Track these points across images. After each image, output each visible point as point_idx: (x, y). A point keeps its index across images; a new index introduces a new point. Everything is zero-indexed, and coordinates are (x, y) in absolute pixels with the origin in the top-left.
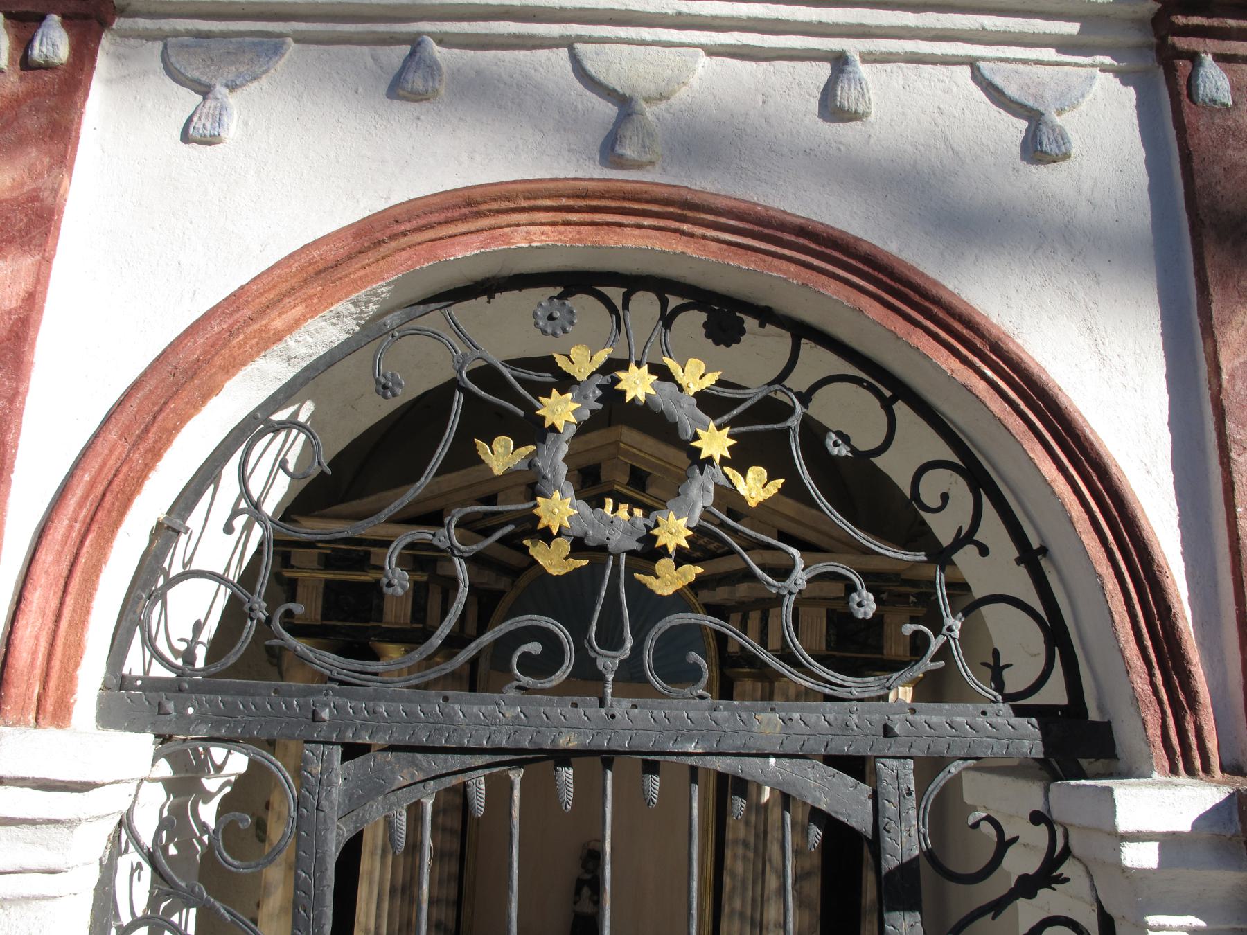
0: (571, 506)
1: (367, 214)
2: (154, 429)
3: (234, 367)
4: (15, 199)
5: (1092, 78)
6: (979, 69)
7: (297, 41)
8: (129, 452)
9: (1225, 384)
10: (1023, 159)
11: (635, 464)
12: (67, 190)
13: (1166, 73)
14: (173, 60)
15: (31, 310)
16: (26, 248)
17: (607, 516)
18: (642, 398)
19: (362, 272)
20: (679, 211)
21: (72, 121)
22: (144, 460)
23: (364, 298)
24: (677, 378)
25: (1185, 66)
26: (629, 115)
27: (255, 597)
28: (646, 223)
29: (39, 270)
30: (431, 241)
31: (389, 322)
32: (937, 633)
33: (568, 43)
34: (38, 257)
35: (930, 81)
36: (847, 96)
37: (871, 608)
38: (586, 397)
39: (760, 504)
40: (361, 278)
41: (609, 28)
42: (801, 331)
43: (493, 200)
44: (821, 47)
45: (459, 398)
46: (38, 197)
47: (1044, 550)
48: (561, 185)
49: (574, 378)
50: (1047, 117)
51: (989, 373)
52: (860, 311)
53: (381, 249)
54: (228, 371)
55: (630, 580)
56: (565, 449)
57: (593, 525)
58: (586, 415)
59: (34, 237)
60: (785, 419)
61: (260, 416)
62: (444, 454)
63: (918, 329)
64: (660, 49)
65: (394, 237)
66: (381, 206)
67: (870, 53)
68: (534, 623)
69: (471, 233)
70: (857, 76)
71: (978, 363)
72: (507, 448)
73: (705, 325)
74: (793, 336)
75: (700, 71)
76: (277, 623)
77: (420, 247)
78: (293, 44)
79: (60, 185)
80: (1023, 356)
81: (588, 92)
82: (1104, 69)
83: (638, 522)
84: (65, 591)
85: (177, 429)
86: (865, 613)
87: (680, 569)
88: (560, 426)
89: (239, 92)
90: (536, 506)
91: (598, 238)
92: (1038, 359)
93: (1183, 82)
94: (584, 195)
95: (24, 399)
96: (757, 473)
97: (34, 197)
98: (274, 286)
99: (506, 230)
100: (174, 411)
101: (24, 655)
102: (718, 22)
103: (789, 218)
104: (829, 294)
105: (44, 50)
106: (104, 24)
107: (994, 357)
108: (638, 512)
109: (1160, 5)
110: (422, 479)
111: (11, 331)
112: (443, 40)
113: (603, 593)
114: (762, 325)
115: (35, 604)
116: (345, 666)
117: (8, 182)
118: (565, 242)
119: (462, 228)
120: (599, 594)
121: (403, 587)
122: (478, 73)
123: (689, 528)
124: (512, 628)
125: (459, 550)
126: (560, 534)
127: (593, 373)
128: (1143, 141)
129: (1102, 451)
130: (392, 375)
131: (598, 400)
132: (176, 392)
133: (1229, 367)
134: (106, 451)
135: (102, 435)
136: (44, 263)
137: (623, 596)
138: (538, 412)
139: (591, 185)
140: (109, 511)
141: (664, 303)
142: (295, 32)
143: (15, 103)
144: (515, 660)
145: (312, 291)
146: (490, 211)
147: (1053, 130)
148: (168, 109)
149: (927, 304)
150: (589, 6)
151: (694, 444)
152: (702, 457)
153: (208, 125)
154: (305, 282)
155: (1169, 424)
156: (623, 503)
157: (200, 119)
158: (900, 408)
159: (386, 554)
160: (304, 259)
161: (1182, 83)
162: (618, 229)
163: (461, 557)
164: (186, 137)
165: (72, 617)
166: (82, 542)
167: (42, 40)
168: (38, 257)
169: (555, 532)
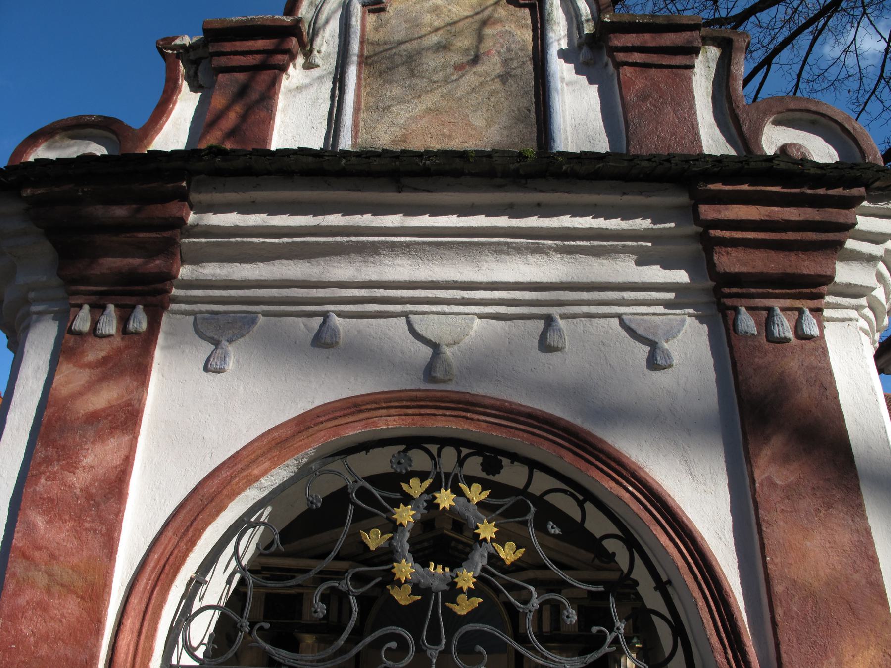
0: (412, 567)
1: (302, 411)
2: (192, 530)
3: (233, 495)
4: (119, 405)
5: (683, 321)
6: (623, 319)
7: (263, 315)
8: (178, 542)
9: (758, 489)
10: (648, 368)
11: (456, 518)
12: (145, 399)
13: (722, 316)
14: (199, 326)
15: (127, 466)
16: (125, 432)
17: (431, 572)
18: (448, 507)
19: (300, 443)
20: (465, 407)
21: (148, 362)
22: (186, 546)
23: (301, 457)
24: (467, 495)
25: (731, 314)
26: (438, 354)
27: (243, 619)
28: (448, 413)
29: (131, 444)
30: (336, 426)
31: (314, 467)
32: (611, 631)
33: (406, 314)
34: (131, 437)
35: (597, 327)
36: (553, 339)
37: (574, 619)
38: (418, 507)
39: (512, 563)
40: (299, 447)
41: (427, 306)
42: (533, 465)
43: (368, 404)
44: (539, 313)
45: (351, 508)
46: (131, 403)
47: (669, 582)
48: (403, 395)
49: (412, 496)
50: (659, 345)
51: (630, 488)
52: (561, 457)
53: (310, 431)
54: (230, 498)
55: (444, 607)
56: (408, 535)
57: (423, 577)
58: (419, 516)
59: (129, 426)
60: (525, 515)
61: (245, 519)
62: (344, 539)
63: (592, 466)
64: (454, 316)
65: (316, 424)
66: (310, 407)
67: (565, 314)
68: (393, 631)
69: (357, 421)
70: (558, 328)
71: (625, 483)
72: (377, 535)
73: (482, 464)
74: (529, 468)
75: (475, 327)
76: (255, 633)
77: (330, 429)
78: (262, 317)
79: (142, 397)
80: (648, 479)
81: (417, 341)
82: (690, 315)
83: (447, 575)
84: (143, 619)
85: (204, 529)
86: (571, 621)
87: (470, 600)
88: (405, 523)
89: (233, 344)
90: (393, 567)
91: (423, 422)
92: (657, 479)
93: (730, 322)
94: (416, 399)
95: (123, 514)
96: (510, 545)
97: (129, 404)
98: (254, 452)
99: (375, 419)
100: (202, 519)
101: (122, 655)
102: (484, 302)
103: (522, 409)
104: (544, 449)
105: (135, 325)
106: (164, 308)
107: (633, 480)
108: (447, 569)
109: (715, 283)
110: (333, 553)
111: (117, 477)
112: (340, 314)
113: (430, 614)
114: (512, 462)
115: (128, 627)
116: (292, 657)
117: (115, 396)
118: (406, 425)
119: (352, 418)
120: (427, 614)
121: (323, 613)
122: (359, 331)
123: (474, 577)
124: (381, 634)
125: (352, 592)
126: (407, 581)
127: (422, 494)
128: (712, 354)
129: (692, 529)
130: (316, 496)
131: (425, 508)
132: (204, 509)
133: (760, 480)
134: (166, 542)
135: (165, 533)
136: (134, 440)
137: (440, 616)
138: (394, 516)
139: (419, 394)
140: (168, 574)
141: (459, 453)
142: (263, 311)
143: (119, 353)
144: (383, 652)
145: (274, 454)
146: (366, 409)
147: (663, 352)
148: (197, 353)
149: (596, 452)
150: (416, 296)
151: (476, 531)
152: (481, 538)
153: (218, 363)
154: (270, 450)
155: (731, 511)
156: (439, 564)
157: (214, 359)
158: (588, 506)
159: (314, 593)
160: (270, 437)
161: (730, 323)
162: (433, 417)
163: (354, 596)
164: (206, 369)
165: (147, 633)
166: (153, 592)
167: (134, 320)
168: (131, 437)
169: (403, 581)
